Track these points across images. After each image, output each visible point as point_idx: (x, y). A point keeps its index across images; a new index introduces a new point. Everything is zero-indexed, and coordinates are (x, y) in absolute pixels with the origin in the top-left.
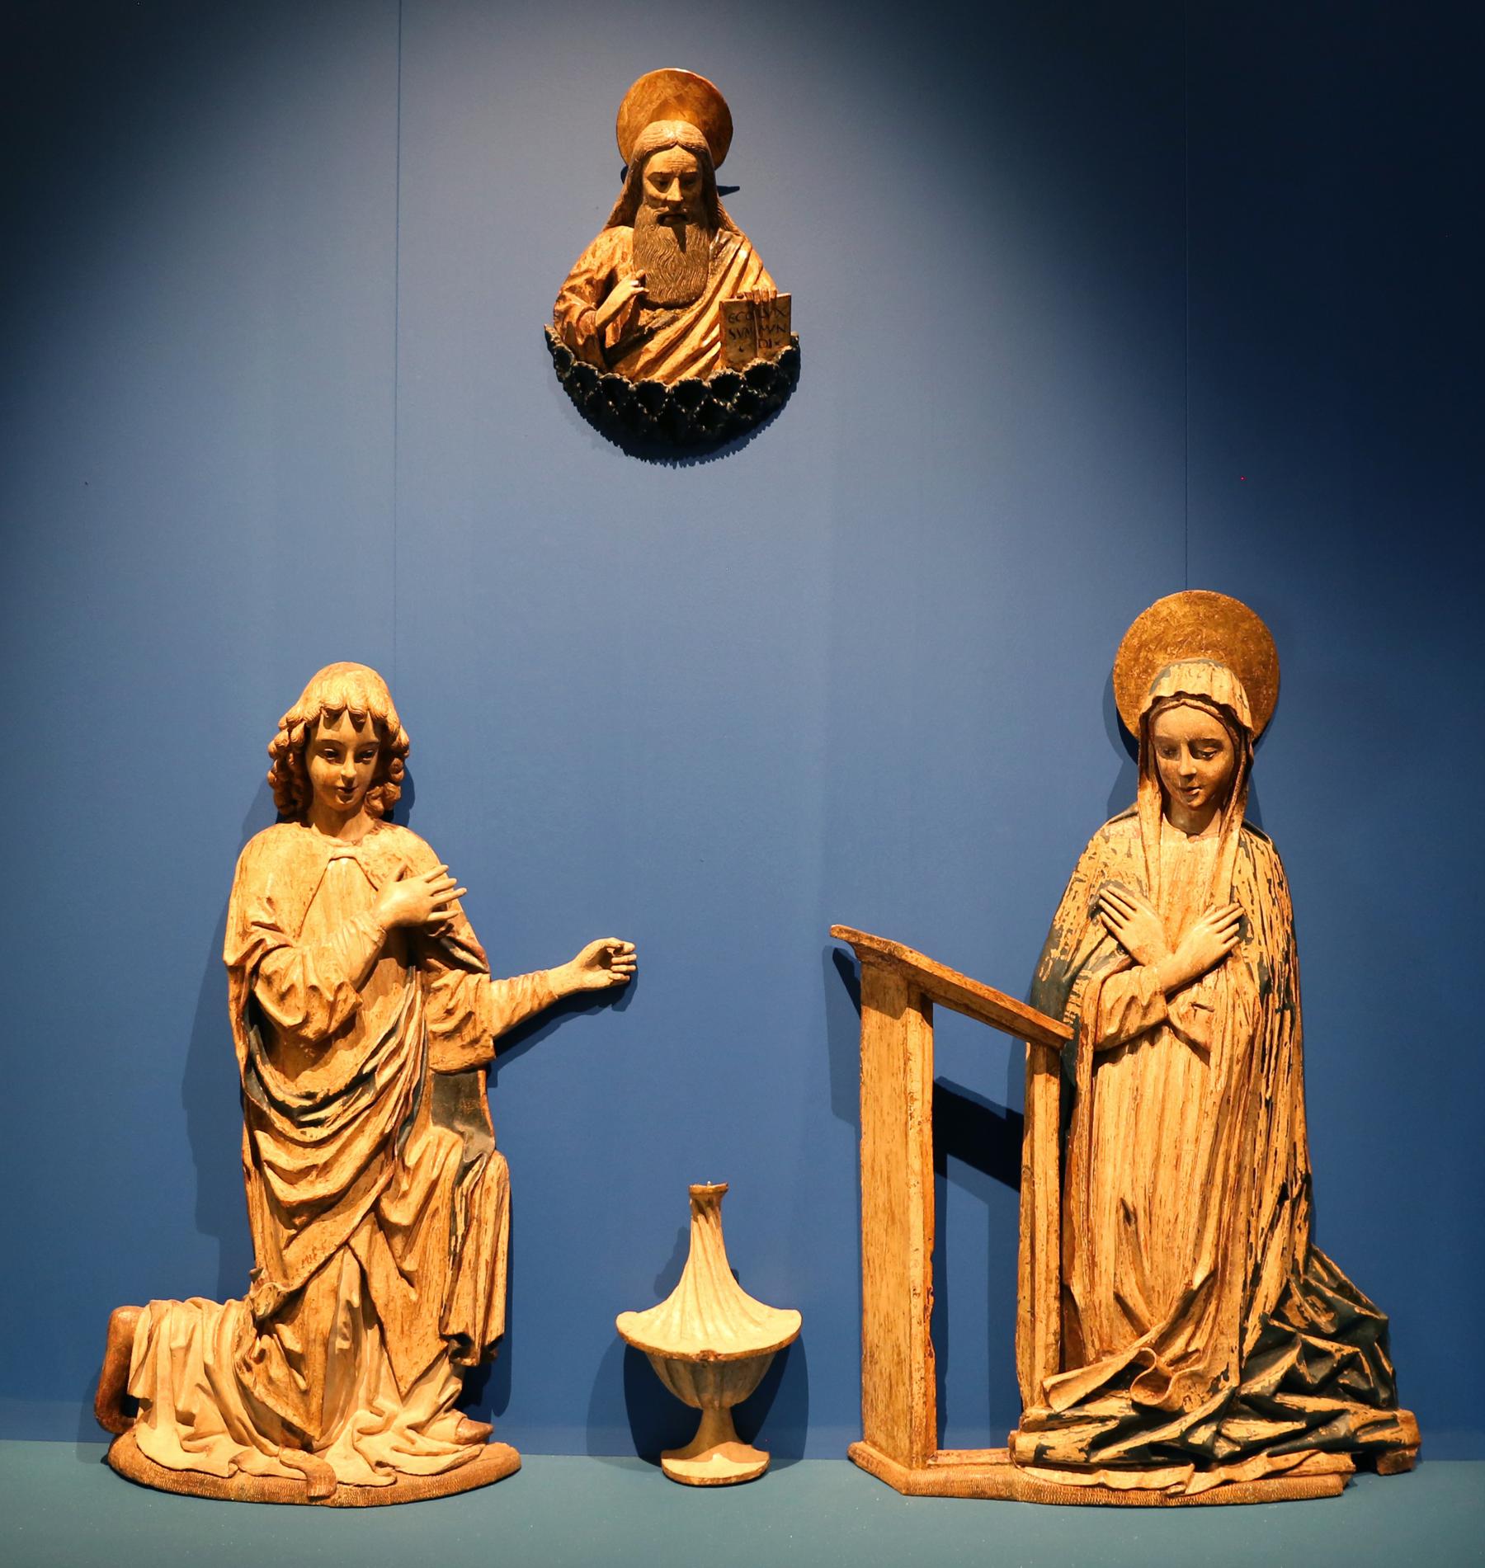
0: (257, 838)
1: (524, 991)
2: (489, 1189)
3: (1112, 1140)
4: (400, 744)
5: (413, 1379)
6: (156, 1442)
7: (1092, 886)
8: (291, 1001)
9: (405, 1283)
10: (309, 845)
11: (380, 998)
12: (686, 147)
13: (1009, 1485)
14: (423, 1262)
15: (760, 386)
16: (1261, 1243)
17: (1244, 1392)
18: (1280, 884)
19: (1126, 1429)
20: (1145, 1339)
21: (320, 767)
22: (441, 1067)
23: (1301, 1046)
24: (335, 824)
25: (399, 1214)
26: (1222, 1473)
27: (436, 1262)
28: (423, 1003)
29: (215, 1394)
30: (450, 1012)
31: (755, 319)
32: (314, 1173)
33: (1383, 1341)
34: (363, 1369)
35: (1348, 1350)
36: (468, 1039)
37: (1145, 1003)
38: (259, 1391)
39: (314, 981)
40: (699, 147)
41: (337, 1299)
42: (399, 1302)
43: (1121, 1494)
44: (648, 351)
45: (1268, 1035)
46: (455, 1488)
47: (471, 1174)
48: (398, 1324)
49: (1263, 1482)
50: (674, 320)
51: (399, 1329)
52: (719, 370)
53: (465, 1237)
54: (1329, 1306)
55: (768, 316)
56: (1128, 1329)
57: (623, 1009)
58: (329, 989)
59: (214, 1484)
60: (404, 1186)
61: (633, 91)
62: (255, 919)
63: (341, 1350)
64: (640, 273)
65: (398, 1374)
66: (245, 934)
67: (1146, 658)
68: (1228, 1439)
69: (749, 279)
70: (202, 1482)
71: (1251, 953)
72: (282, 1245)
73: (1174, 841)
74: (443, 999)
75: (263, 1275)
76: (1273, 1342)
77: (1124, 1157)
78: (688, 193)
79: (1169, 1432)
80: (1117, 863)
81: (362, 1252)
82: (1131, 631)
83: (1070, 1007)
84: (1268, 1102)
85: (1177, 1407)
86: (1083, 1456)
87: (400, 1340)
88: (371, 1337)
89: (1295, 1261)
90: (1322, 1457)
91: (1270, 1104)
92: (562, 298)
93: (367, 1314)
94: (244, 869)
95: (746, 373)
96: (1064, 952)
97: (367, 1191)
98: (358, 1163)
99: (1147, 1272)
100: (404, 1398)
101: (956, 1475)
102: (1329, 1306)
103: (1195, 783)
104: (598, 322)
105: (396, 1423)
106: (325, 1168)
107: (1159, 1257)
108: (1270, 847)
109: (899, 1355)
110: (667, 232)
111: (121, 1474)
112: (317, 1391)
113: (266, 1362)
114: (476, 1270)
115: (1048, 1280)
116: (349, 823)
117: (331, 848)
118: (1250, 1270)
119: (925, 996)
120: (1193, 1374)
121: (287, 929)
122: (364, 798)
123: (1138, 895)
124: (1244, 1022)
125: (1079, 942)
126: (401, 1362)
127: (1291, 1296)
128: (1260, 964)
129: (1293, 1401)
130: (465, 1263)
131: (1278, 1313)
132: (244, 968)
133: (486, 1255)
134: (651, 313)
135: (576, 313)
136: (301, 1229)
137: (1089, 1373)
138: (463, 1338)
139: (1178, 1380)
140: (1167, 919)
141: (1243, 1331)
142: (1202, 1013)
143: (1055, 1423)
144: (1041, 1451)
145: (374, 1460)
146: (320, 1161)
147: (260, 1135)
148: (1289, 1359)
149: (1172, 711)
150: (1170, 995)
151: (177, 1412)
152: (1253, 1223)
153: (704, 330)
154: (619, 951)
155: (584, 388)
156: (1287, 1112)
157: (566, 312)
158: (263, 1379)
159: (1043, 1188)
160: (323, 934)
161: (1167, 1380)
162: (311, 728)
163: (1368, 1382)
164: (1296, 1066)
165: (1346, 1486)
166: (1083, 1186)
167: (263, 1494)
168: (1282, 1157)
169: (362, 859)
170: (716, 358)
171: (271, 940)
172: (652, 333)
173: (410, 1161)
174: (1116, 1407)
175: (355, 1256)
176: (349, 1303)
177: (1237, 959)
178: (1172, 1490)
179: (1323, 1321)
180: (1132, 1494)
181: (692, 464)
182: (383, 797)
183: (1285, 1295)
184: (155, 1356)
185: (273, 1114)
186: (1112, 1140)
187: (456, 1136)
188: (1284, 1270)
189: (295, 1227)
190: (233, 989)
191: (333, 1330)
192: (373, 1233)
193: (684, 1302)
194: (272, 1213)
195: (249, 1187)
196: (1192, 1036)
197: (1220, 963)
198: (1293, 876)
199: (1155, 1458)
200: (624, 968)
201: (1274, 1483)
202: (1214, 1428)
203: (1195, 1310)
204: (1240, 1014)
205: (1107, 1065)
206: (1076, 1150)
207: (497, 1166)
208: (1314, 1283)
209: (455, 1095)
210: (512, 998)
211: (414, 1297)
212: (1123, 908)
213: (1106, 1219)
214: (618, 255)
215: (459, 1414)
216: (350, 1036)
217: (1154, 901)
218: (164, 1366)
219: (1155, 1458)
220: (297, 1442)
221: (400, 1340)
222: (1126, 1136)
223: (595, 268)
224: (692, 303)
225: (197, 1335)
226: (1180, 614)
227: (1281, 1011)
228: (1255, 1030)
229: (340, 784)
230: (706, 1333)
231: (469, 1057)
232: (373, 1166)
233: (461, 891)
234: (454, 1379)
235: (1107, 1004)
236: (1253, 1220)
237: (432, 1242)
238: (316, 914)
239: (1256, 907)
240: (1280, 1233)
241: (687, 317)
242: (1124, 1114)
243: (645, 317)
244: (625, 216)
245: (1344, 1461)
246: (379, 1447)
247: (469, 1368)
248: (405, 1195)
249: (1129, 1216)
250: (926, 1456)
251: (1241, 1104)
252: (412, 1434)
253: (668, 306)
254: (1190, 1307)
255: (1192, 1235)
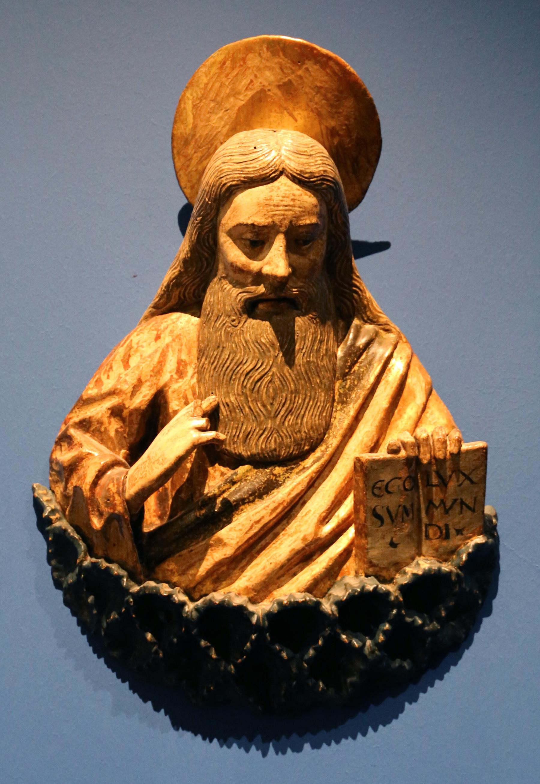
12: (300, 180)
15: (427, 609)
31: (421, 490)
40: (323, 178)
44: (220, 542)
50: (271, 486)
52: (353, 580)
55: (444, 483)
61: (203, 75)
64: (208, 403)
69: (409, 411)
78: (302, 261)
92: (65, 439)
95: (403, 588)
104: (131, 491)
110: (261, 330)
134: (229, 472)
135: (89, 471)
153: (324, 505)
155: (103, 606)
157: (72, 468)
170: (346, 554)
172: (230, 510)
181: (298, 749)
214: (171, 365)
223: (127, 388)
224: (304, 456)
241: (293, 483)
243: (216, 479)
244: (185, 295)
253: (259, 462)
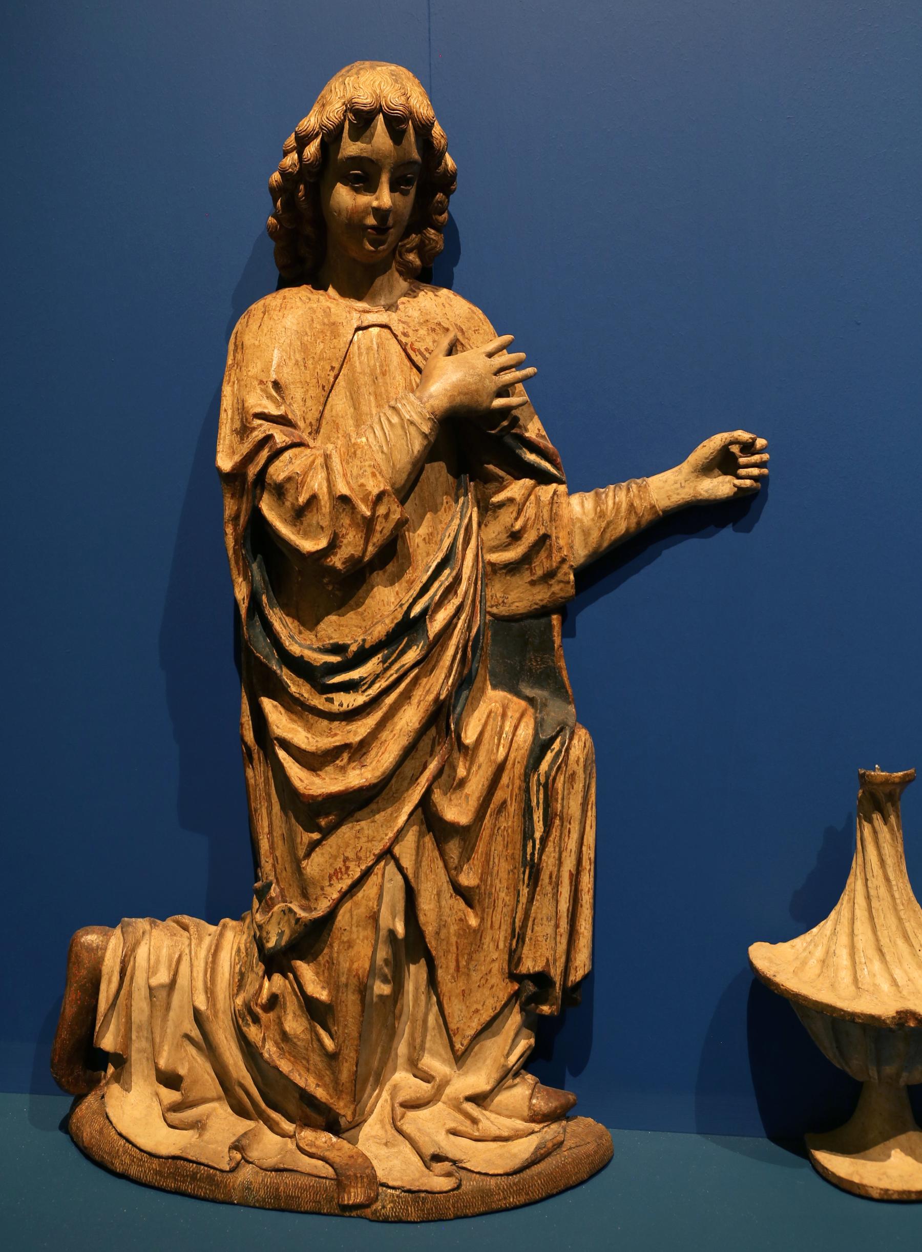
0: (257, 307)
1: (617, 506)
2: (573, 775)
4: (446, 170)
5: (471, 1032)
6: (135, 1113)
8: (312, 518)
9: (462, 904)
10: (327, 312)
11: (429, 515)
14: (486, 873)
21: (344, 197)
22: (502, 610)
24: (358, 286)
25: (456, 811)
27: (503, 875)
28: (479, 525)
29: (209, 1048)
30: (515, 536)
32: (346, 756)
34: (404, 1018)
36: (539, 572)
38: (270, 1050)
39: (342, 488)
41: (377, 928)
42: (453, 928)
46: (534, 1191)
47: (549, 756)
48: (452, 957)
51: (452, 965)
53: (544, 840)
57: (748, 530)
58: (365, 500)
59: (211, 1179)
60: (461, 772)
62: (258, 410)
63: (381, 997)
65: (453, 1026)
66: (244, 431)
70: (193, 1177)
72: (301, 853)
74: (506, 517)
75: (274, 892)
81: (407, 862)
87: (455, 979)
88: (416, 974)
93: (413, 946)
94: (240, 347)
97: (414, 780)
98: (404, 741)
100: (460, 1058)
105: (449, 1091)
106: (358, 751)
111: (86, 1153)
112: (349, 1054)
113: (277, 1009)
114: (557, 885)
116: (378, 282)
117: (355, 315)
121: (301, 424)
122: (396, 252)
126: (454, 1008)
130: (545, 877)
132: (244, 475)
133: (569, 864)
136: (327, 833)
138: (542, 979)
145: (429, 1150)
146: (355, 739)
147: (268, 704)
151: (158, 1071)
154: (748, 448)
158: (273, 1033)
160: (351, 429)
162: (331, 138)
167: (277, 1197)
169: (398, 328)
171: (280, 437)
173: (469, 737)
175: (400, 869)
176: (392, 933)
182: (420, 249)
184: (130, 995)
185: (286, 675)
187: (523, 703)
189: (319, 829)
190: (230, 507)
191: (373, 971)
192: (421, 835)
193: (852, 934)
194: (283, 808)
195: (250, 773)
200: (755, 471)
207: (580, 744)
209: (515, 650)
210: (601, 515)
211: (473, 922)
215: (530, 1078)
216: (390, 568)
218: (140, 1006)
220: (320, 1120)
221: (455, 979)
225: (184, 968)
229: (371, 221)
230: (895, 983)
231: (541, 595)
232: (421, 744)
233: (530, 370)
234: (525, 1031)
237: (498, 847)
238: (339, 402)
246: (431, 1125)
247: (542, 1017)
248: (462, 783)
252: (470, 1107)
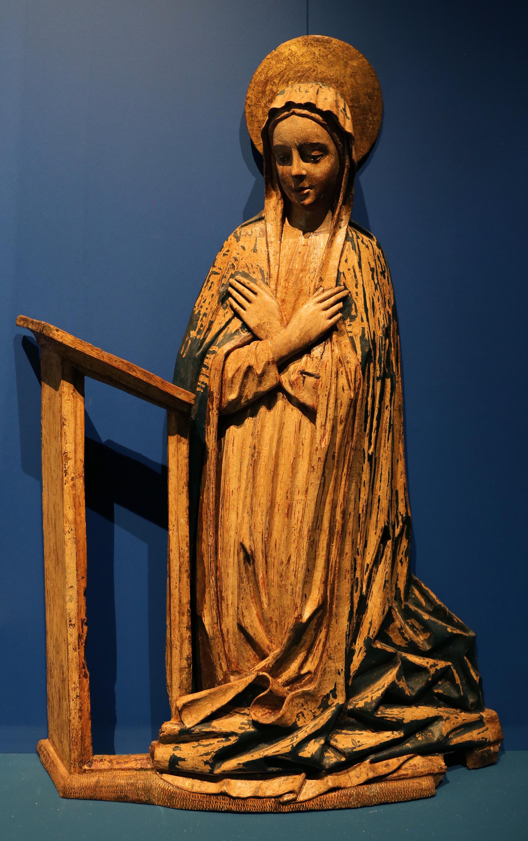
3: (235, 492)
7: (224, 277)
13: (148, 790)
16: (366, 577)
17: (350, 707)
18: (383, 273)
19: (245, 743)
20: (263, 663)
23: (403, 410)
26: (330, 781)
33: (472, 654)
35: (442, 664)
37: (259, 372)
43: (240, 802)
45: (370, 399)
49: (365, 787)
54: (426, 627)
56: (250, 653)
67: (272, 90)
68: (336, 750)
71: (355, 328)
73: (294, 237)
76: (376, 663)
77: (244, 506)
79: (283, 747)
80: (246, 258)
82: (259, 70)
83: (202, 378)
84: (370, 457)
85: (290, 723)
86: (208, 768)
89: (397, 589)
90: (418, 760)
91: (373, 460)
96: (199, 332)
99: (265, 606)
101: (104, 779)
102: (426, 627)
103: (306, 184)
107: (274, 592)
108: (374, 243)
109: (63, 674)
115: (181, 614)
118: (356, 601)
119: (77, 370)
120: (305, 694)
123: (260, 282)
124: (346, 388)
125: (211, 323)
127: (393, 621)
128: (362, 338)
129: (394, 713)
131: (382, 634)
137: (215, 694)
139: (292, 700)
140: (283, 301)
141: (349, 654)
142: (310, 380)
143: (187, 737)
144: (174, 760)
148: (389, 677)
149: (284, 122)
150: (282, 363)
152: (359, 561)
156: (389, 465)
159: (176, 534)
161: (283, 699)
163: (458, 691)
164: (398, 426)
165: (439, 785)
166: (211, 531)
168: (384, 503)
174: (236, 723)
177: (341, 333)
178: (286, 798)
179: (421, 639)
180: (250, 803)
183: (388, 619)
186: (235, 492)
188: (386, 600)
196: (302, 400)
197: (325, 336)
198: (390, 267)
199: (271, 769)
201: (376, 788)
202: (322, 742)
203: (307, 638)
204: (343, 381)
205: (233, 428)
206: (205, 501)
208: (413, 608)
212: (246, 292)
213: (231, 560)
217: (273, 287)
219: (271, 769)
222: (246, 488)
226: (299, 53)
227: (383, 379)
228: (356, 394)
235: (229, 374)
236: (359, 558)
239: (360, 289)
240: (383, 569)
242: (245, 469)
245: (438, 762)
249: (249, 558)
250: (82, 762)
251: (340, 461)
254: (301, 636)
255: (301, 575)
